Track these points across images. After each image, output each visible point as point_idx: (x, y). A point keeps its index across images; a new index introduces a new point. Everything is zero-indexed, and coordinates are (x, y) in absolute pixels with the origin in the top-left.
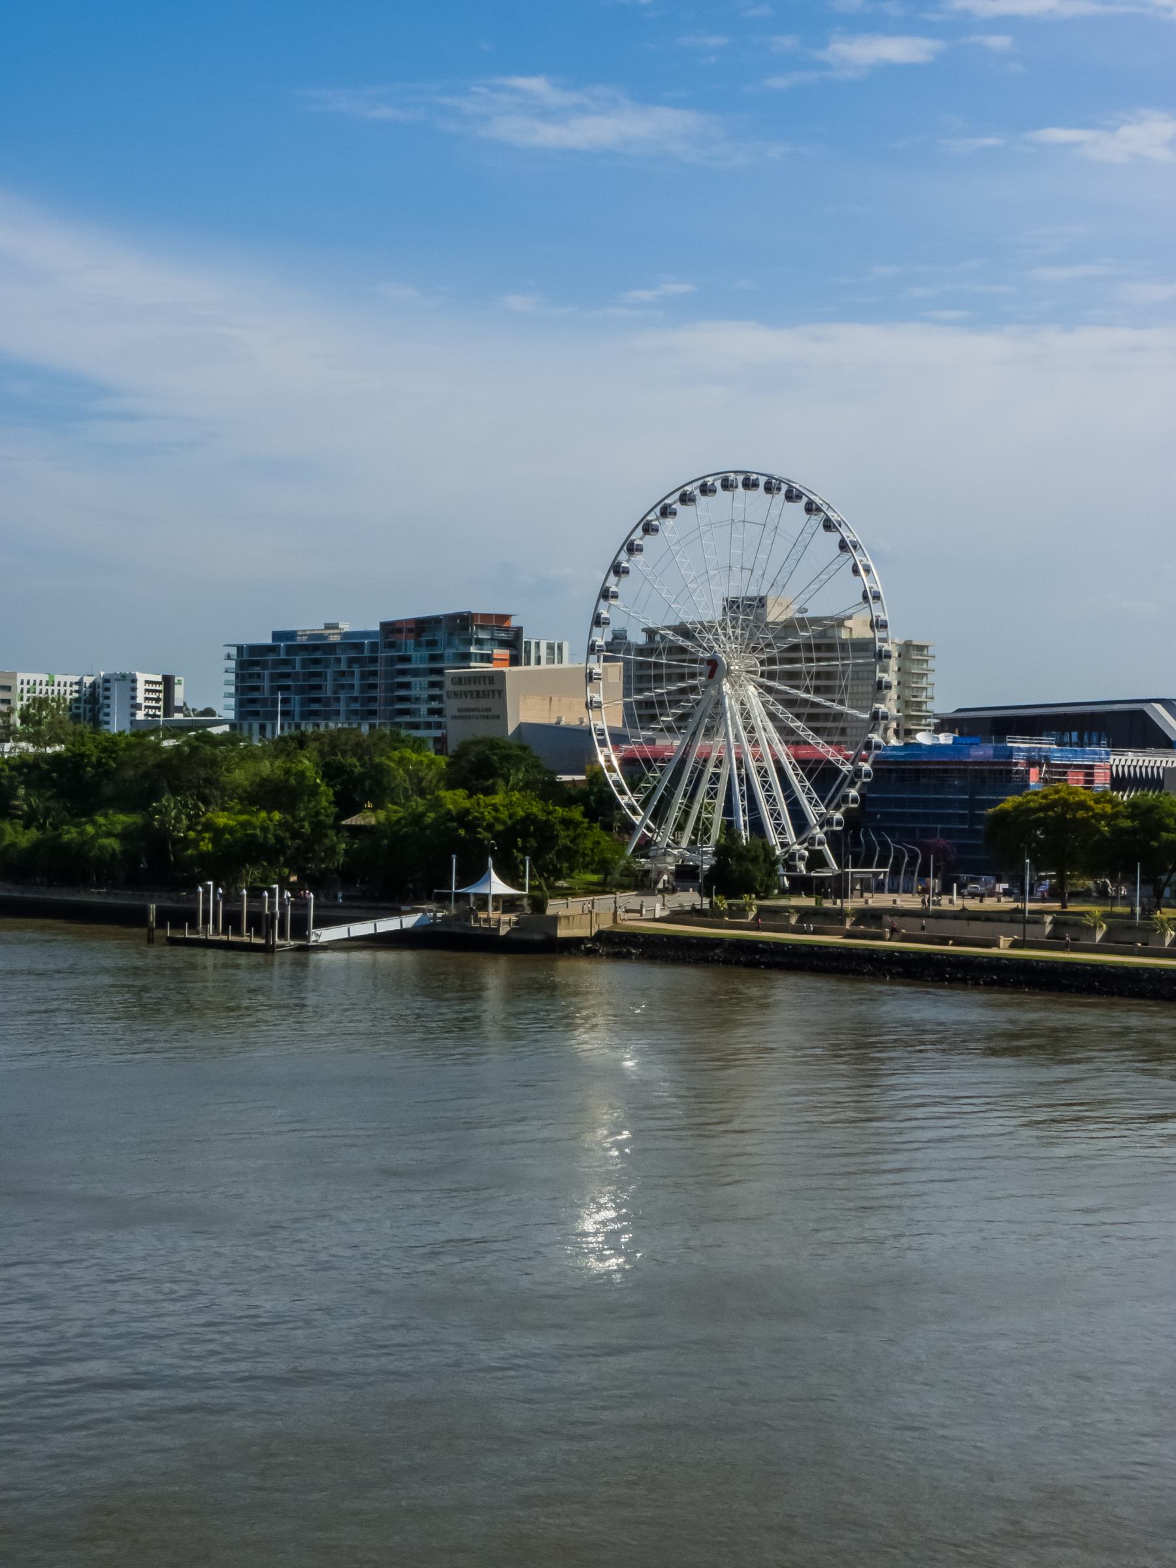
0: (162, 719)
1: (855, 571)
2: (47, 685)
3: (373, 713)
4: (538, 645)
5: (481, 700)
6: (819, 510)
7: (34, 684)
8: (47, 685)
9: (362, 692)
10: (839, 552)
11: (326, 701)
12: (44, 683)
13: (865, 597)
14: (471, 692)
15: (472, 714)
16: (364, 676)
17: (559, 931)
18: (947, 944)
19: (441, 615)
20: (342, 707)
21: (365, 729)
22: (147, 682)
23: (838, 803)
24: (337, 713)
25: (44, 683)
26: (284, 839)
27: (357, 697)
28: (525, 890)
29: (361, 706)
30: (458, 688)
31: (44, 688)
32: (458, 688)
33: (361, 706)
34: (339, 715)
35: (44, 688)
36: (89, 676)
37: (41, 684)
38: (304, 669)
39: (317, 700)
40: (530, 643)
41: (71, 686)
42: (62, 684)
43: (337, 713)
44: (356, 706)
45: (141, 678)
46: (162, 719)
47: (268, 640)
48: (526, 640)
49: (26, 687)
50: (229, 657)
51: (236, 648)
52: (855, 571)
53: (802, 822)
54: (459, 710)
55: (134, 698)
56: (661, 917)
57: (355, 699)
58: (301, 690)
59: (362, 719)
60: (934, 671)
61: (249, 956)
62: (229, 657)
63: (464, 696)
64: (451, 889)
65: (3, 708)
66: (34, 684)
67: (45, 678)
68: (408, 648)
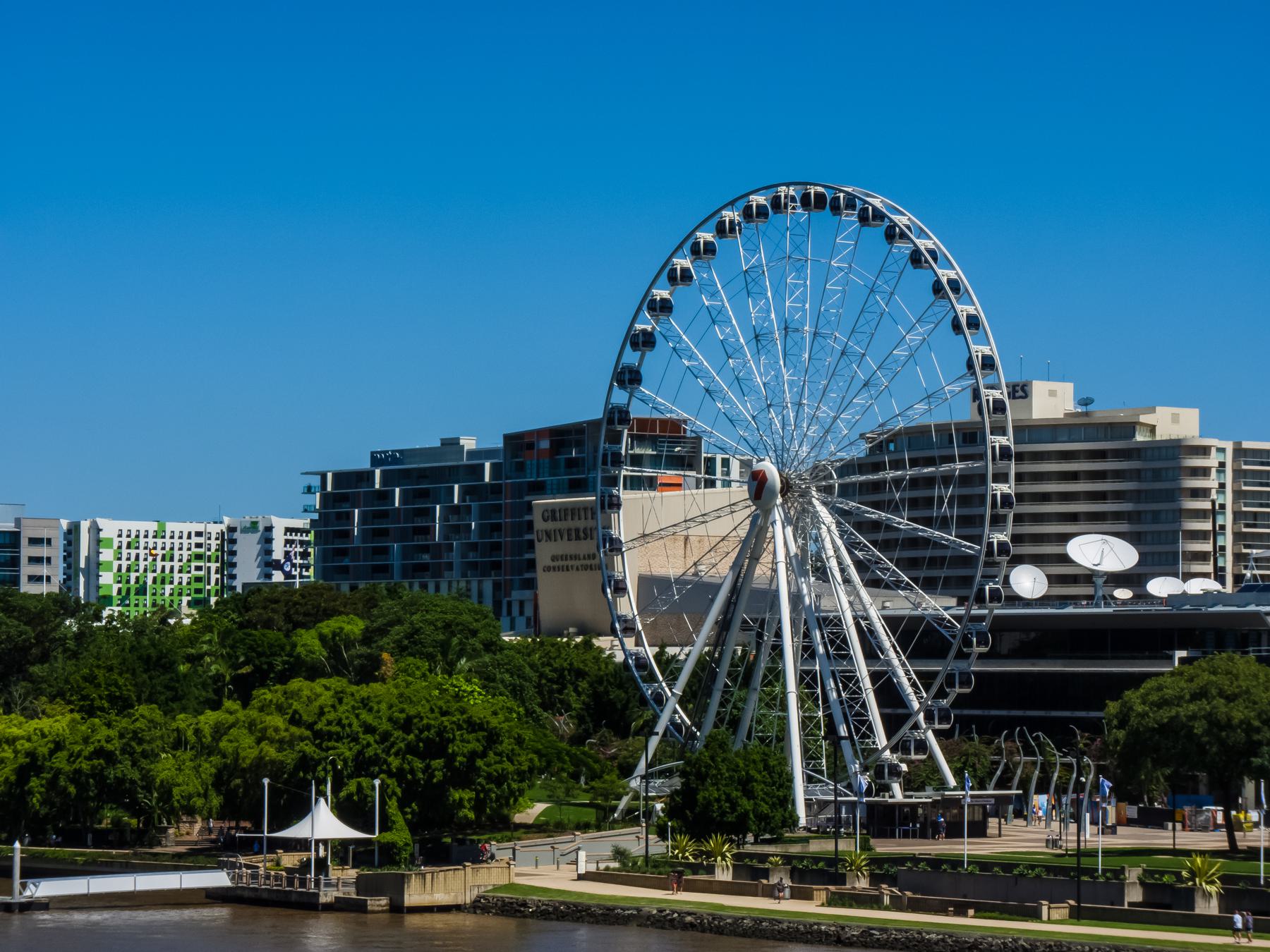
0: (298, 580)
1: (956, 326)
2: (155, 537)
3: (497, 566)
4: (726, 463)
5: (583, 542)
6: (903, 236)
7: (137, 536)
8: (155, 537)
9: (482, 535)
10: (933, 298)
11: (436, 550)
12: (151, 535)
13: (970, 365)
14: (569, 530)
15: (570, 563)
16: (484, 512)
17: (406, 897)
18: (965, 915)
19: (584, 422)
20: (455, 557)
21: (345, 587)
22: (289, 530)
23: (941, 688)
24: (450, 566)
25: (151, 535)
26: (429, 731)
27: (476, 544)
28: (373, 833)
29: (432, 558)
30: (550, 525)
31: (151, 541)
32: (550, 525)
33: (432, 558)
34: (452, 570)
35: (151, 541)
36: (215, 523)
37: (146, 536)
38: (404, 505)
39: (425, 549)
40: (715, 459)
41: (189, 537)
42: (177, 535)
43: (450, 566)
44: (472, 557)
45: (280, 525)
46: (298, 580)
47: (366, 465)
48: (705, 455)
49: (125, 540)
50: (309, 490)
51: (319, 477)
52: (956, 326)
53: (900, 711)
54: (554, 558)
55: (269, 552)
56: (587, 873)
57: (474, 547)
58: (403, 535)
59: (483, 575)
60: (302, 474)
61: (820, 843)
62: (309, 490)
63: (559, 537)
64: (263, 833)
65: (6, 573)
66: (137, 536)
67: (152, 526)
68: (541, 471)
